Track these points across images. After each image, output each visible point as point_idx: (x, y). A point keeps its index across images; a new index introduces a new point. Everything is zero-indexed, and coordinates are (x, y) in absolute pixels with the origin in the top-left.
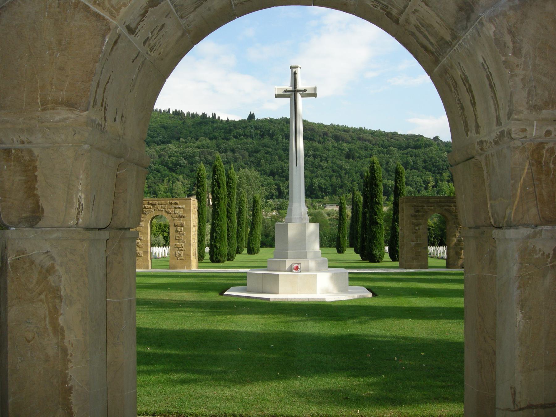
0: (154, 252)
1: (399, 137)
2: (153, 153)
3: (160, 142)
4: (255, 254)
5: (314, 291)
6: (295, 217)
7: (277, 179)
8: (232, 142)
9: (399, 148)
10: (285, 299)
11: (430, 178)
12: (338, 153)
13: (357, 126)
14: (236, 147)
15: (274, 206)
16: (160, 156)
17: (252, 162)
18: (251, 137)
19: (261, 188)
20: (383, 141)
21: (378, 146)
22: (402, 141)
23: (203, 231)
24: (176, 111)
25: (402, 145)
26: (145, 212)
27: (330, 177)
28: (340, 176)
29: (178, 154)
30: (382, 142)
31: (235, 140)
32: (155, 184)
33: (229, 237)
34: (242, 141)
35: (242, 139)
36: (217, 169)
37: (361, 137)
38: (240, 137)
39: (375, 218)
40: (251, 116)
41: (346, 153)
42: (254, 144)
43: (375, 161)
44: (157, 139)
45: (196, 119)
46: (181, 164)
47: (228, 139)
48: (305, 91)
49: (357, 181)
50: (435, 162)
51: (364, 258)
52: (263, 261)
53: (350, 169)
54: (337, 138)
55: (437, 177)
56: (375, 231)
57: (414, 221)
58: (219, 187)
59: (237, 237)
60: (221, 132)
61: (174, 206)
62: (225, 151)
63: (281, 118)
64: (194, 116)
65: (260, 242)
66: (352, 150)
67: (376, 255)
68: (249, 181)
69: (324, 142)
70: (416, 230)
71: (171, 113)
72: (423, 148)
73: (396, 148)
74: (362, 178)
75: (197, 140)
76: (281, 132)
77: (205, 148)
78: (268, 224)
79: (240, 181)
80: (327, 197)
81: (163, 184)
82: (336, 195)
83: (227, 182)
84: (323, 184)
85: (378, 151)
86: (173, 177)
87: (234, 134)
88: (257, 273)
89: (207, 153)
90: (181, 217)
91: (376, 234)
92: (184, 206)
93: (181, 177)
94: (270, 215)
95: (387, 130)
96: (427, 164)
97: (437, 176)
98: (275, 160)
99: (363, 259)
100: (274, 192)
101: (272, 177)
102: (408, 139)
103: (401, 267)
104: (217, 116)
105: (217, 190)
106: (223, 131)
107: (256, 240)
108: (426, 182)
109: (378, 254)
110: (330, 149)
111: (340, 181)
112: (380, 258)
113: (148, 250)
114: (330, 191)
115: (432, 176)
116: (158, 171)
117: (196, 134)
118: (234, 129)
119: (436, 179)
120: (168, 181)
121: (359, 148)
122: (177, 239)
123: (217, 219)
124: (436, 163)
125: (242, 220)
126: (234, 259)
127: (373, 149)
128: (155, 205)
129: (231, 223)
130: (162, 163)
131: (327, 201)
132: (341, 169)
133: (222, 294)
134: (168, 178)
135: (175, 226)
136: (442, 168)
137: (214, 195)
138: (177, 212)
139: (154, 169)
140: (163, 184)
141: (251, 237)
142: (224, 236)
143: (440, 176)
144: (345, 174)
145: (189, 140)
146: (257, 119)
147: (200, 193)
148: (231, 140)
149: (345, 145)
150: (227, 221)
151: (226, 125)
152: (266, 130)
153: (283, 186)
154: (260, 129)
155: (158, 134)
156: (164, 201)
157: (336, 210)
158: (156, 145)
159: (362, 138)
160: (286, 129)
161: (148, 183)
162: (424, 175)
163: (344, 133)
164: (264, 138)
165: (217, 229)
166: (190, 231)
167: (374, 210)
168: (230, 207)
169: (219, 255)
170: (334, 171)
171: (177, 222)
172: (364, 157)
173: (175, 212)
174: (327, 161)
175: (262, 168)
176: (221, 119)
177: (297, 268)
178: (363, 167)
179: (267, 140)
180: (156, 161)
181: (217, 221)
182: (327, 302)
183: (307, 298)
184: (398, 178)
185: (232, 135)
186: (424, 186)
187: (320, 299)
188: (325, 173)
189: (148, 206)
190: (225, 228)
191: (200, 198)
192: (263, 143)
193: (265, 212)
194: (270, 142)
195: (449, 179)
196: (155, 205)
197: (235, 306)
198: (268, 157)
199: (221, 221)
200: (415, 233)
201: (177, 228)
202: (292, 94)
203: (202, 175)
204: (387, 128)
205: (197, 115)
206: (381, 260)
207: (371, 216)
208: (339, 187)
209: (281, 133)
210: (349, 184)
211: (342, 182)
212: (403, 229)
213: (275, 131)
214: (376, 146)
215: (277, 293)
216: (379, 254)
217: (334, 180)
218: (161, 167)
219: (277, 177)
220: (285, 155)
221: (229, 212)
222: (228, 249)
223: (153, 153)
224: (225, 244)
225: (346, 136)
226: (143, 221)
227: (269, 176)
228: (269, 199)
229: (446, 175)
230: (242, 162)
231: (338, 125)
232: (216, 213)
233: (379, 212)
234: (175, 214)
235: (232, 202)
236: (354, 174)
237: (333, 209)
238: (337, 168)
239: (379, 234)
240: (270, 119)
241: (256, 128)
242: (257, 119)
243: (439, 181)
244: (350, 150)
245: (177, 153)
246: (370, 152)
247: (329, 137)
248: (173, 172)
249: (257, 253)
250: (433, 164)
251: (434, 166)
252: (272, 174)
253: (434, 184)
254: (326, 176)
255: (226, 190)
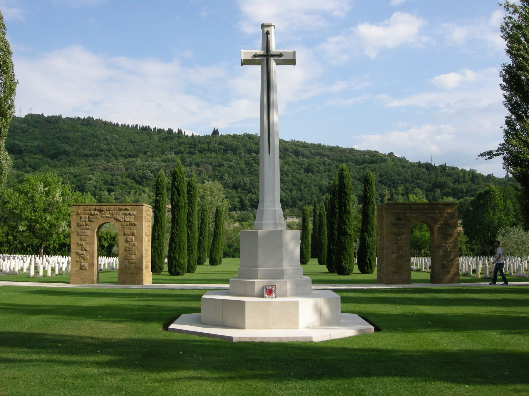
0: (103, 264)
1: (356, 153)
2: (120, 166)
3: (127, 156)
4: (217, 265)
5: (295, 325)
6: (267, 222)
7: (240, 192)
8: (197, 157)
9: (356, 163)
10: (255, 337)
11: (385, 191)
12: (297, 168)
13: (316, 142)
14: (200, 161)
15: (236, 218)
16: (127, 169)
17: (216, 175)
18: (214, 152)
19: (225, 200)
20: (341, 157)
21: (335, 161)
22: (359, 156)
23: (162, 241)
24: (143, 126)
25: (359, 160)
26: (91, 219)
27: (291, 191)
28: (300, 190)
29: (145, 168)
30: (339, 157)
31: (200, 154)
32: (122, 195)
33: (190, 247)
34: (206, 155)
35: (206, 154)
36: (177, 176)
37: (320, 152)
38: (204, 151)
39: (345, 228)
40: (215, 132)
41: (305, 167)
42: (217, 159)
43: (344, 168)
44: (124, 153)
45: (163, 134)
46: (147, 177)
47: (192, 154)
48: (281, 55)
49: (316, 195)
50: (390, 177)
51: (331, 270)
52: (225, 273)
53: (310, 183)
54: (297, 153)
55: (392, 191)
56: (344, 242)
57: (395, 230)
58: (179, 195)
59: (199, 248)
60: (186, 146)
61: (124, 212)
62: (190, 165)
63: (243, 134)
64: (160, 131)
65: (222, 252)
66: (311, 165)
67: (346, 267)
68: (212, 193)
69: (284, 157)
70: (398, 240)
71: (138, 128)
72: (379, 163)
73: (353, 163)
74: (320, 192)
75: (163, 154)
76: (243, 147)
77: (170, 162)
78: (230, 235)
79: (204, 193)
80: (288, 209)
81: (129, 196)
82: (296, 208)
83: (188, 191)
84: (284, 197)
85: (336, 165)
86: (139, 190)
87: (198, 148)
88: (215, 299)
89: (172, 167)
90: (132, 225)
91: (346, 245)
92: (135, 213)
93: (147, 189)
94: (232, 227)
95: (344, 147)
96: (382, 178)
97: (392, 190)
98: (238, 174)
99: (330, 271)
100: (237, 204)
101: (235, 190)
102: (364, 155)
103: (379, 281)
104: (183, 131)
105: (176, 198)
106: (188, 146)
107: (218, 251)
108: (382, 195)
109: (347, 265)
110: (291, 164)
111: (300, 194)
112: (349, 270)
113: (94, 262)
114: (291, 204)
115: (388, 190)
116: (125, 184)
117: (162, 149)
118: (199, 144)
119: (391, 192)
120: (134, 193)
121: (317, 163)
122: (127, 250)
123: (176, 228)
124: (391, 177)
125: (204, 231)
126: (195, 270)
127: (331, 164)
128: (102, 211)
129: (191, 233)
130: (129, 176)
131: (287, 214)
132: (301, 183)
133: (166, 327)
134: (134, 191)
135: (124, 235)
136: (397, 182)
137: (174, 203)
138: (128, 219)
139: (121, 181)
140: (129, 196)
141: (213, 247)
142: (183, 247)
143: (395, 190)
144: (305, 188)
145: (155, 154)
146: (221, 135)
147: (159, 201)
148: (196, 154)
149: (305, 160)
150: (187, 231)
151: (191, 140)
152: (229, 146)
153: (245, 199)
154: (224, 144)
155: (126, 148)
156: (113, 207)
157: (296, 222)
158: (123, 158)
159: (321, 153)
160: (249, 144)
161: (115, 195)
162: (379, 188)
163: (304, 148)
164: (227, 153)
165: (177, 240)
166: (142, 241)
167: (344, 220)
168: (191, 216)
169: (179, 266)
170: (294, 185)
171: (127, 231)
172: (323, 172)
173: (126, 219)
174: (288, 175)
175: (225, 181)
176: (186, 135)
177: (270, 292)
178: (321, 181)
179: (230, 155)
180: (123, 174)
181: (176, 231)
182: (318, 343)
183: (286, 336)
184: (367, 186)
185: (197, 149)
186: (380, 199)
187: (305, 337)
188: (285, 186)
189: (95, 212)
190: (184, 238)
191: (159, 206)
192: (226, 158)
193: (228, 223)
194: (233, 157)
195: (404, 192)
196: (102, 211)
197: (181, 353)
198: (231, 171)
199: (181, 231)
200: (397, 243)
201: (127, 238)
202: (263, 60)
203: (161, 182)
204: (344, 145)
205: (163, 130)
206: (351, 273)
207: (340, 226)
208: (299, 200)
209: (244, 149)
210: (309, 197)
211: (302, 195)
212: (382, 239)
213: (238, 146)
214: (334, 161)
215: (243, 328)
216: (349, 266)
217: (295, 193)
218: (128, 181)
219: (239, 190)
220: (247, 169)
221: (190, 222)
222: (188, 260)
223: (120, 166)
224: (185, 255)
225: (305, 152)
226: (89, 229)
227: (231, 189)
228: (232, 211)
229: (401, 189)
230: (206, 176)
231: (298, 142)
232: (175, 222)
233: (349, 222)
234: (125, 221)
235: (193, 211)
236: (313, 188)
237: (293, 221)
238: (297, 181)
239: (348, 245)
240: (233, 134)
241: (220, 143)
242: (221, 135)
243: (395, 195)
244: (309, 164)
245: (143, 167)
246: (328, 167)
247: (289, 152)
248: (139, 185)
249: (220, 263)
250: (388, 179)
251: (389, 180)
252: (235, 187)
253: (390, 197)
254: (286, 189)
255: (186, 198)
